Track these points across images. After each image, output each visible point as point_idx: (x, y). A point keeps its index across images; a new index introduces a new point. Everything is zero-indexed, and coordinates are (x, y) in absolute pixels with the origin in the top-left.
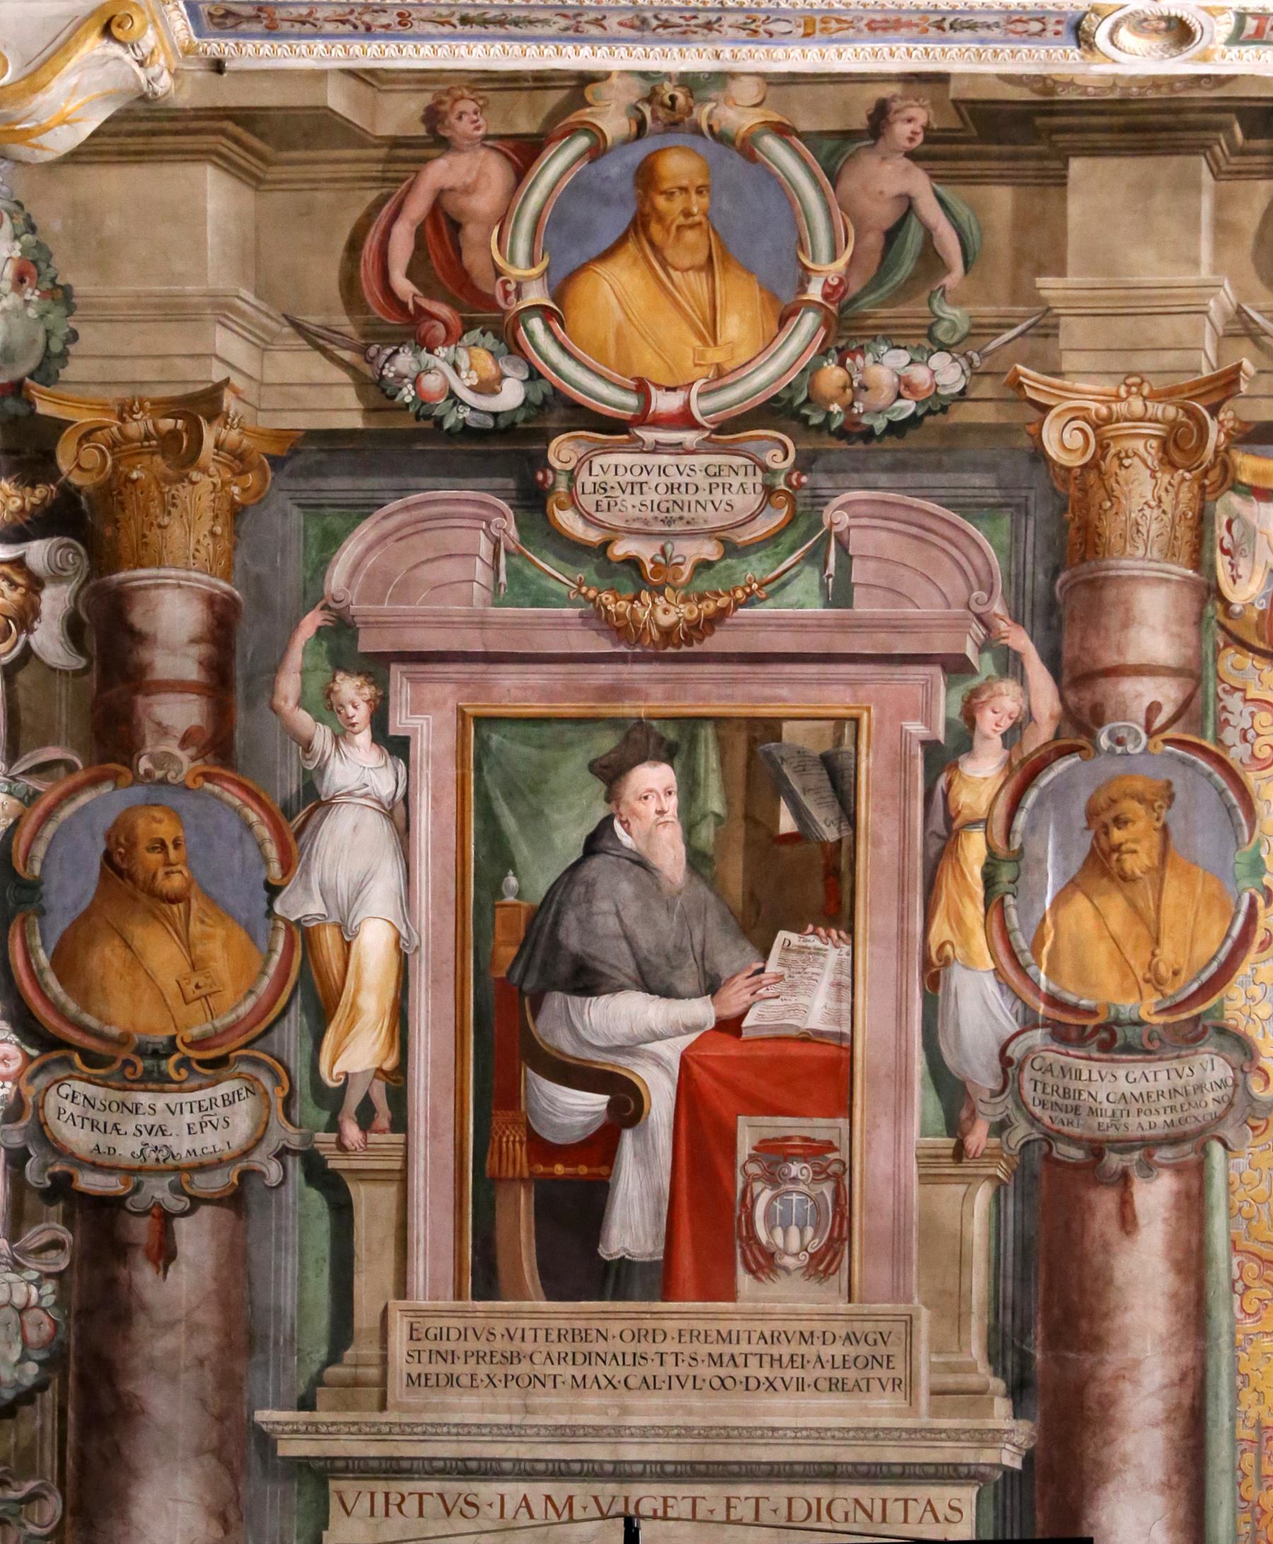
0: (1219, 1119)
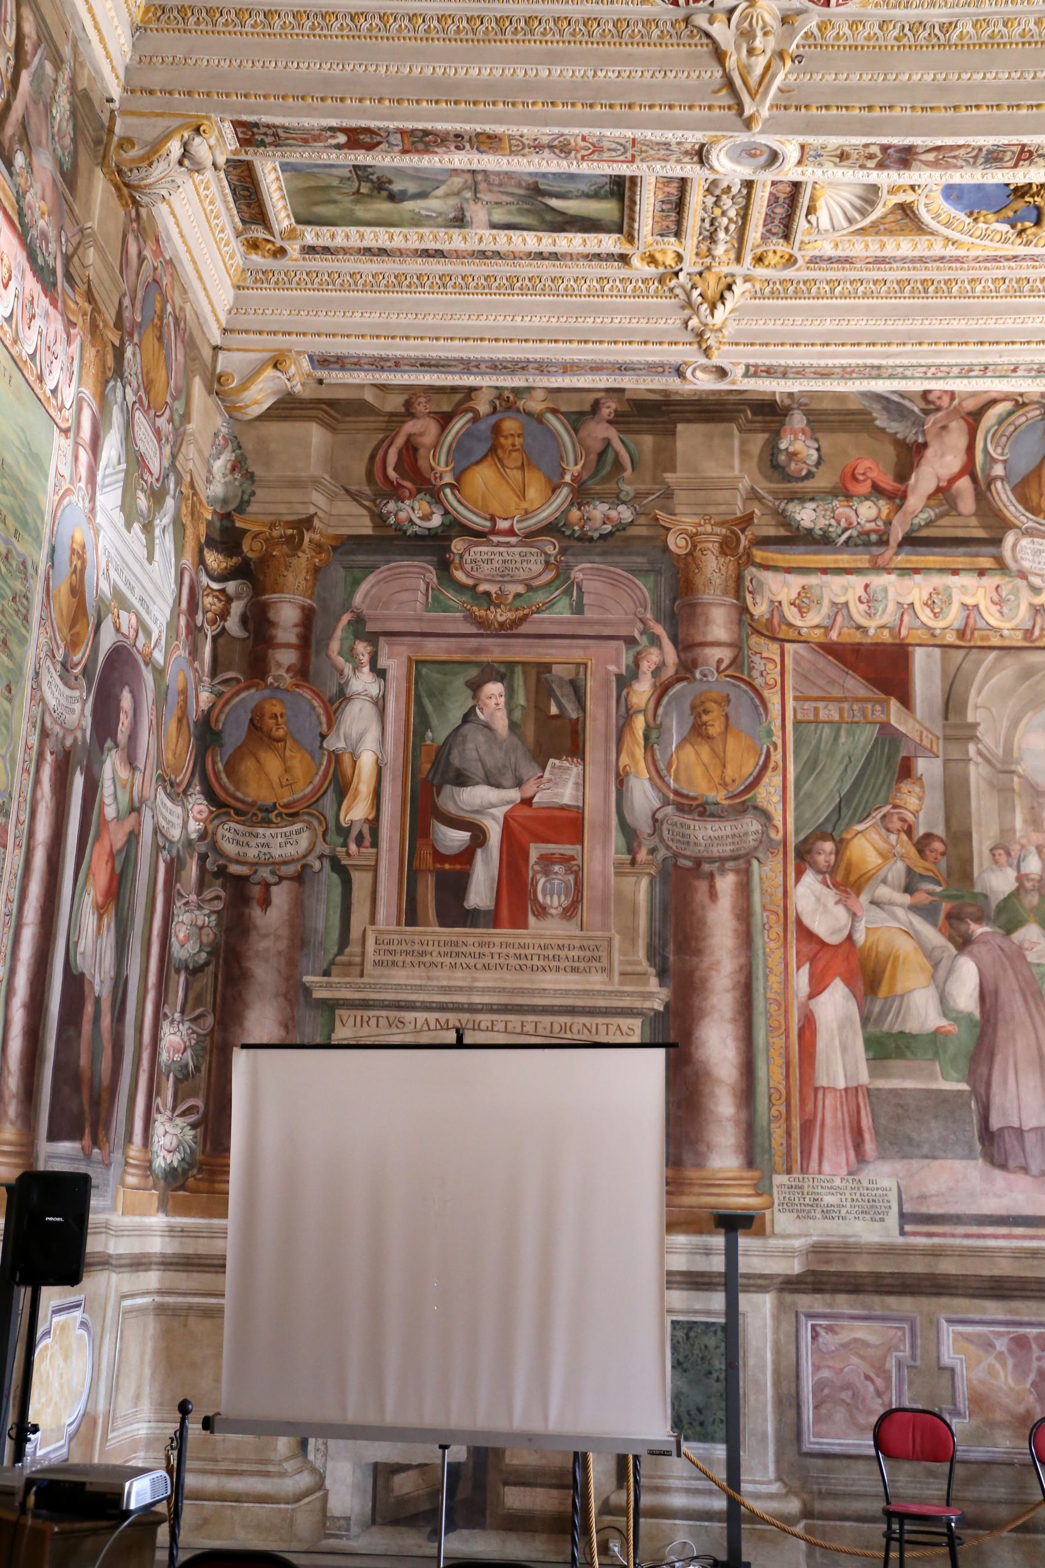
0: (756, 849)
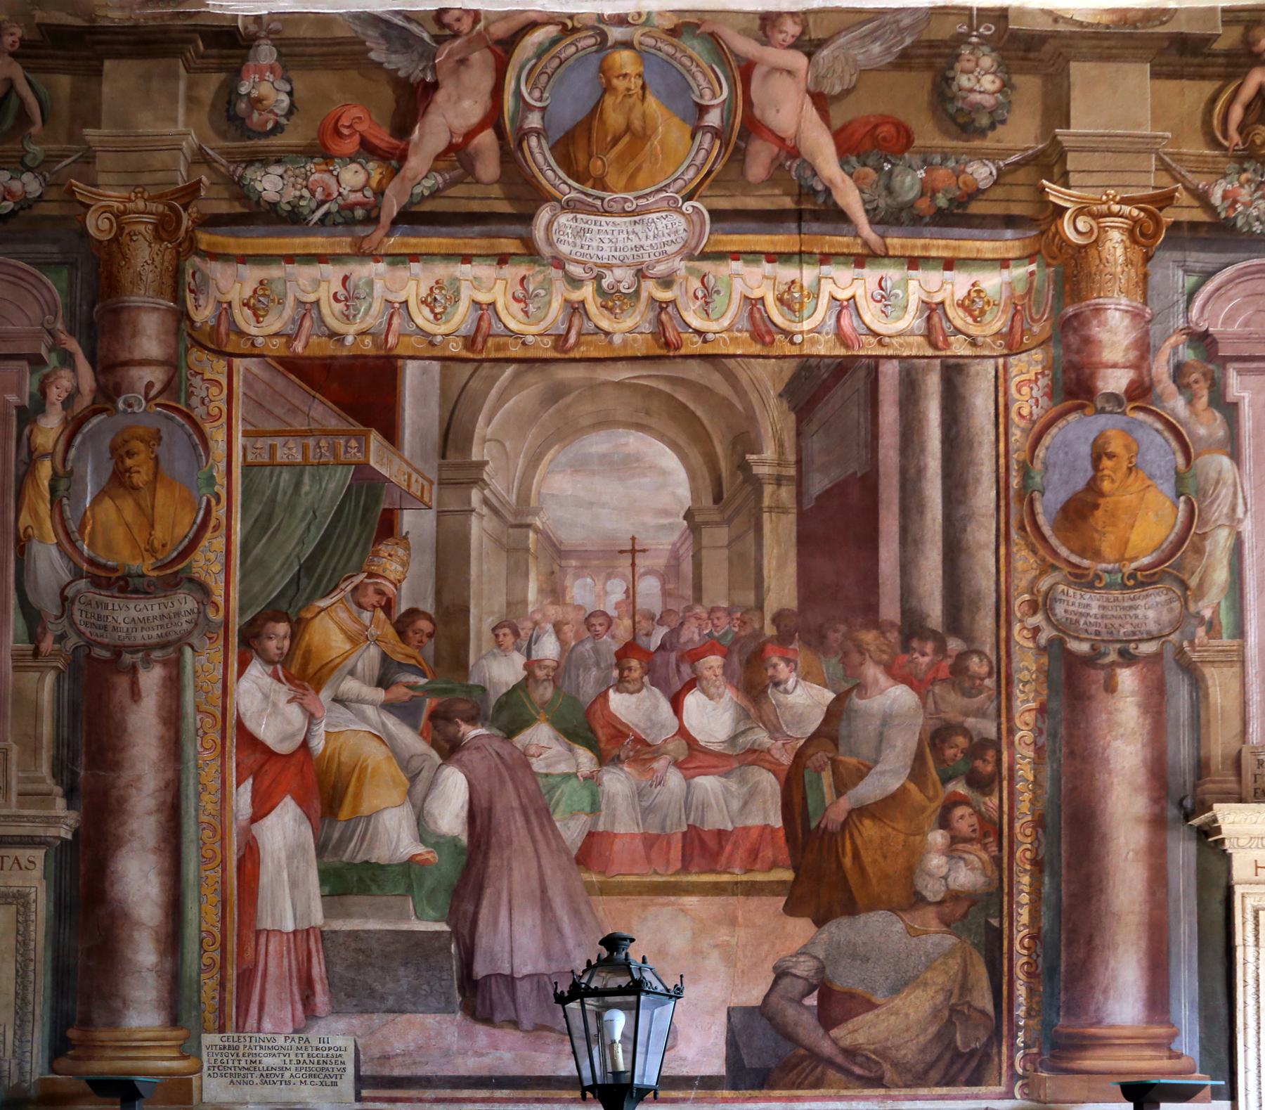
0: (190, 633)
